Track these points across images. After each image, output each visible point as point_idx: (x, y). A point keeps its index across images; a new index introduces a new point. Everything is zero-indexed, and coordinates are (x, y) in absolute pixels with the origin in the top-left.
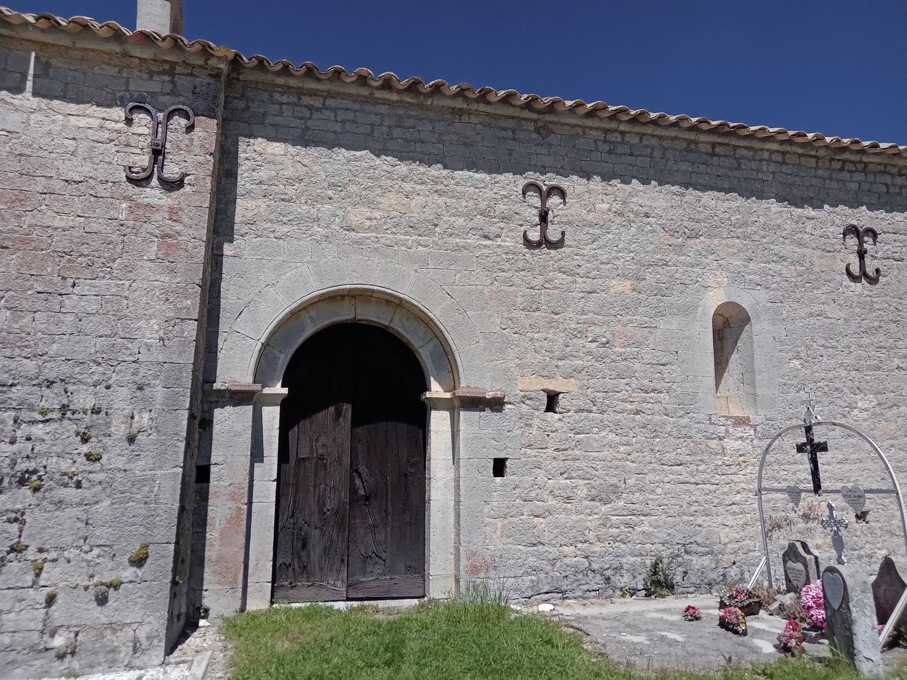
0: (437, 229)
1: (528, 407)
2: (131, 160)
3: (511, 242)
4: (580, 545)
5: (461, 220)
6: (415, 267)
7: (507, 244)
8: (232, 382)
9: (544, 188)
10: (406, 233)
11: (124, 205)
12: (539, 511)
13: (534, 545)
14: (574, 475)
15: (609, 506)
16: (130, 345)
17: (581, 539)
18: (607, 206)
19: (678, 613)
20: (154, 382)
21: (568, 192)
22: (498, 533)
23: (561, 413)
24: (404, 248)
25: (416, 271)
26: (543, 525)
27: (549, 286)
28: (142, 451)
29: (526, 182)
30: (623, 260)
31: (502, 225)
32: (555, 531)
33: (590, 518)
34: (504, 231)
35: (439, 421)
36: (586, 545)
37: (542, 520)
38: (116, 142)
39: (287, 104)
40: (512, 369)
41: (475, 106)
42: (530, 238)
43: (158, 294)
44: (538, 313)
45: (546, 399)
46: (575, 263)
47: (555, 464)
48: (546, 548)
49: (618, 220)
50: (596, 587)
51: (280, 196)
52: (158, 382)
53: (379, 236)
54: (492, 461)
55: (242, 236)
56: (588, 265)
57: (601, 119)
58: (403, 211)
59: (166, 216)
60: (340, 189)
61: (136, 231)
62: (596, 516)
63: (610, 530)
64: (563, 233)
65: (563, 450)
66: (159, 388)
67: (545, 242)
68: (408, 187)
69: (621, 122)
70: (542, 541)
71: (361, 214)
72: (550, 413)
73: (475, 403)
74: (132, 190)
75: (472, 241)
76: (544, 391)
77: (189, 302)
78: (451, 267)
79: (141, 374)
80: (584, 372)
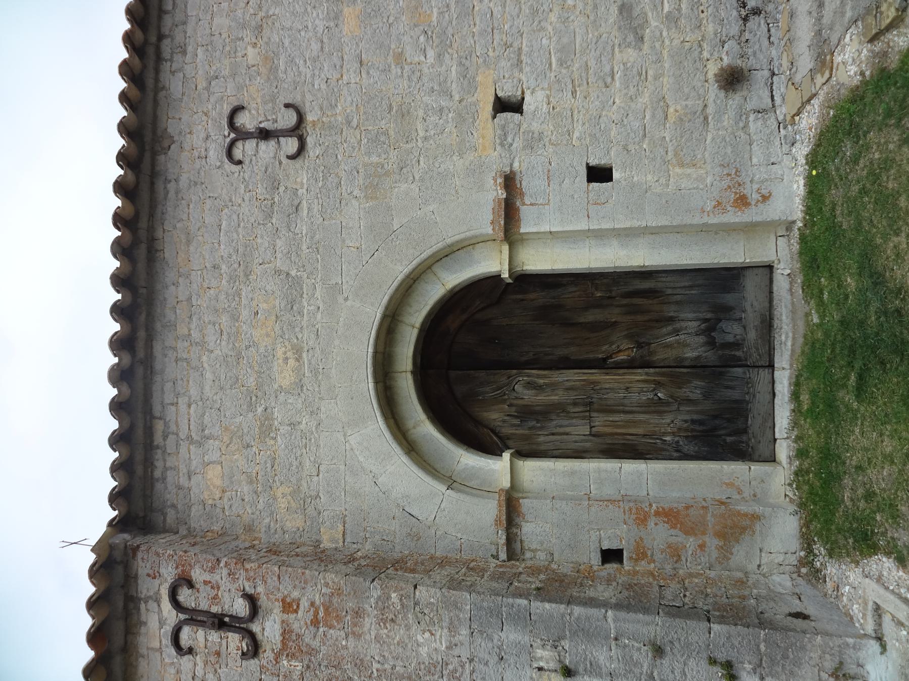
0: (293, 273)
1: (517, 139)
2: (235, 654)
3: (300, 175)
4: (706, 54)
5: (279, 243)
6: (340, 299)
7: (305, 181)
8: (496, 525)
9: (233, 135)
10: (301, 313)
11: (285, 662)
12: (660, 114)
13: (706, 118)
14: (607, 69)
15: (650, 14)
16: (451, 667)
17: (696, 52)
18: (250, 49)
19: (539, 236)
20: (495, 641)
21: (236, 104)
22: (689, 171)
23: (523, 93)
24: (319, 316)
25: (346, 299)
26: (679, 108)
27: (355, 121)
28: (585, 659)
29: (226, 160)
30: (317, 22)
31: (282, 189)
32: (686, 90)
33: (667, 42)
34: (289, 186)
35: (539, 260)
36: (705, 45)
37: (671, 110)
38: (217, 666)
39: (165, 461)
40: (467, 163)
41: (142, 234)
42: (296, 149)
43: (386, 631)
44: (392, 133)
45: (505, 114)
46: (324, 86)
47: (593, 95)
48: (710, 103)
49: (266, 32)
50: (764, 27)
51: (269, 469)
52: (496, 637)
53: (306, 349)
54: (607, 566)
55: (320, 513)
56: (326, 68)
57: (144, 67)
58: (274, 318)
59: (293, 616)
60: (254, 398)
61: (312, 652)
62: (665, 34)
63: (684, 11)
64: (287, 106)
65: (574, 87)
66: (503, 635)
67: (297, 130)
68: (245, 314)
69: (146, 42)
70: (700, 109)
71: (282, 372)
72: (525, 107)
73: (509, 212)
74: (267, 655)
75: (304, 228)
76: (494, 117)
77: (393, 595)
78: (339, 253)
79: (487, 657)
80: (467, 63)
